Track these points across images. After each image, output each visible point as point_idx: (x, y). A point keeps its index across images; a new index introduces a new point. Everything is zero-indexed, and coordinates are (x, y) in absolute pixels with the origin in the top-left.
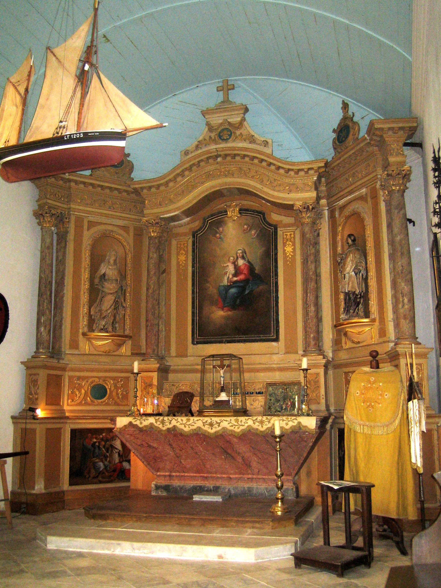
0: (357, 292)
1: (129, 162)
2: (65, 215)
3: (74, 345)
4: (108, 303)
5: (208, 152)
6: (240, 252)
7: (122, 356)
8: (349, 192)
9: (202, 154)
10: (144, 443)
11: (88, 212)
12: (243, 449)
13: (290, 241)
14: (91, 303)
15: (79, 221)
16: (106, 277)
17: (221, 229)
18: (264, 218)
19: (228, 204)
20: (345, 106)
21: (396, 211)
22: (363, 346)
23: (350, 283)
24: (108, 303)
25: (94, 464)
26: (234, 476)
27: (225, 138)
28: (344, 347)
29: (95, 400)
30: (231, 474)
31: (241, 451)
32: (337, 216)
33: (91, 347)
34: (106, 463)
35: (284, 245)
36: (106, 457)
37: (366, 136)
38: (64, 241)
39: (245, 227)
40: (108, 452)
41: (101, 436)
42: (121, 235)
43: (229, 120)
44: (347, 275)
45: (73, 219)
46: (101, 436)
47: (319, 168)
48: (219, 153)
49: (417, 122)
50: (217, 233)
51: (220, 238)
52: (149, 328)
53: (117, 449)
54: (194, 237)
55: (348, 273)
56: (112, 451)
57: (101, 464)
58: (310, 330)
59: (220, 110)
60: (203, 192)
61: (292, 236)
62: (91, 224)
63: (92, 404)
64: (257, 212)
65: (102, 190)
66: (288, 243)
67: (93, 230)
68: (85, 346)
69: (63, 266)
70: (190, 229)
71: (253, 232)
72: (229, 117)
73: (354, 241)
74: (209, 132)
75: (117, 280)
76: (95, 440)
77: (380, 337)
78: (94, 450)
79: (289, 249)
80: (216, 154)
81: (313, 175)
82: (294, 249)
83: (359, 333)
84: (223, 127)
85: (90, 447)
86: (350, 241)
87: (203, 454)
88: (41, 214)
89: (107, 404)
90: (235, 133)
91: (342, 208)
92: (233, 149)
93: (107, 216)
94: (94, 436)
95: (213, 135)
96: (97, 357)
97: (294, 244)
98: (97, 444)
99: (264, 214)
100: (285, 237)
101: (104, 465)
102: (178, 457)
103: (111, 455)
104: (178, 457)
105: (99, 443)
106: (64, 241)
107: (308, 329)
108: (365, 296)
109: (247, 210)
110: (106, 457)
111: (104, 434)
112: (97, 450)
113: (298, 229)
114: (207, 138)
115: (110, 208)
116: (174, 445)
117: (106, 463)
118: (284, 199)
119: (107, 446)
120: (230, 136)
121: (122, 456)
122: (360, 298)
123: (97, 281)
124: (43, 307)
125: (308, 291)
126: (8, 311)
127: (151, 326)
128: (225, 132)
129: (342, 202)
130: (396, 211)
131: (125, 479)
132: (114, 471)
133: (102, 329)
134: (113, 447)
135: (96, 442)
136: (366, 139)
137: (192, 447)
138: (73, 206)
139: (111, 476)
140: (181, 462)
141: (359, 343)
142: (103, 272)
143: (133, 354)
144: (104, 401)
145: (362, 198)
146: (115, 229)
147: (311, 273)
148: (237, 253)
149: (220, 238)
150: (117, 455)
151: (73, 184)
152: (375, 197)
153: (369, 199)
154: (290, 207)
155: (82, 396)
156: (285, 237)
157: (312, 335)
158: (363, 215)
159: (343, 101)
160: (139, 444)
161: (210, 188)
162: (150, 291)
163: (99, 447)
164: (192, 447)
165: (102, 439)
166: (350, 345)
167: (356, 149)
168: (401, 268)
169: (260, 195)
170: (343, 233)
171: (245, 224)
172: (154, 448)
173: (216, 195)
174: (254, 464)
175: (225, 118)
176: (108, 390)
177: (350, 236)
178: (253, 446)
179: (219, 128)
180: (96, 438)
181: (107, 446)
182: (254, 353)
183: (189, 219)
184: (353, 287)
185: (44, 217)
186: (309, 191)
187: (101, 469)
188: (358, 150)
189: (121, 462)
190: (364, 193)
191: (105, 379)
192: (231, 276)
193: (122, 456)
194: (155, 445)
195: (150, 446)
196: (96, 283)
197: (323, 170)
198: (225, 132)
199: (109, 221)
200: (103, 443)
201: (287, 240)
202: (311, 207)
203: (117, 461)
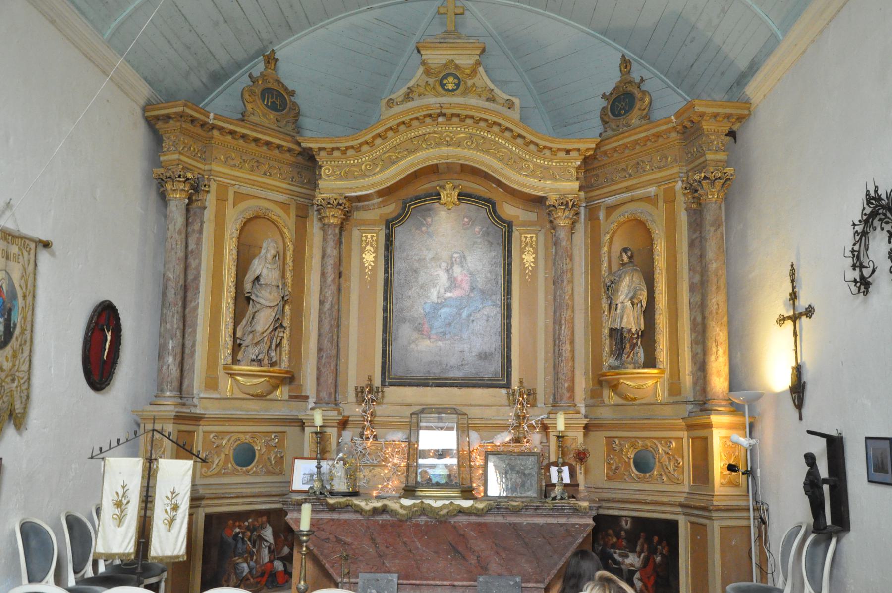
0: (634, 330)
1: (295, 104)
2: (203, 181)
3: (212, 383)
4: (264, 320)
5: (428, 107)
6: (456, 255)
7: (278, 400)
8: (627, 188)
9: (419, 108)
10: (331, 537)
11: (235, 179)
12: (480, 545)
13: (531, 247)
14: (237, 319)
15: (223, 189)
16: (262, 281)
17: (429, 220)
18: (495, 211)
19: (441, 183)
20: (626, 63)
21: (712, 229)
22: (640, 404)
23: (625, 317)
24: (264, 320)
25: (235, 566)
26: (460, 583)
27: (450, 88)
28: (606, 402)
29: (239, 468)
30: (457, 580)
31: (477, 549)
32: (601, 218)
33: (235, 387)
34: (252, 563)
35: (522, 251)
36: (251, 555)
37: (673, 117)
38: (198, 220)
39: (466, 220)
40: (254, 547)
41: (246, 523)
42: (277, 213)
43: (457, 62)
44: (620, 305)
45: (213, 187)
46: (246, 523)
47: (588, 149)
48: (443, 111)
49: (749, 108)
50: (423, 224)
51: (427, 233)
52: (323, 361)
53: (266, 541)
54: (387, 227)
55: (622, 303)
56: (260, 546)
57: (245, 565)
58: (563, 377)
59: (445, 45)
60: (412, 165)
61: (534, 239)
62: (240, 197)
63: (234, 474)
64: (484, 200)
65: (233, 138)
66: (527, 248)
67: (243, 206)
68: (227, 386)
69: (197, 261)
70: (381, 216)
71: (477, 229)
72: (457, 57)
73: (630, 258)
74: (424, 76)
75: (278, 286)
76: (238, 530)
77: (671, 394)
78: (236, 546)
79: (528, 258)
80: (439, 111)
81: (575, 159)
82: (536, 259)
83: (639, 387)
84: (447, 72)
85: (230, 540)
86: (626, 259)
87: (421, 551)
88: (170, 178)
89: (256, 473)
90: (466, 83)
91: (611, 209)
92: (466, 107)
93: (254, 183)
94: (237, 524)
95: (431, 81)
96: (243, 402)
97: (536, 252)
98: (240, 535)
99: (494, 204)
100: (523, 239)
101: (249, 566)
102: (380, 556)
103: (259, 551)
104: (380, 556)
105: (243, 533)
106: (198, 220)
107: (560, 375)
108: (648, 335)
109: (470, 196)
110: (251, 555)
111: (250, 520)
112: (240, 545)
113: (543, 231)
114: (422, 84)
115: (265, 174)
116: (378, 540)
117: (252, 563)
118: (533, 188)
119: (254, 537)
120: (458, 85)
121: (273, 552)
122: (637, 338)
123: (248, 286)
124: (172, 326)
125: (563, 322)
126: (121, 330)
127: (327, 358)
128: (451, 79)
129: (611, 200)
130: (712, 229)
131: (276, 586)
132: (263, 574)
133: (253, 361)
134: (261, 539)
135: (239, 533)
136: (671, 122)
137: (405, 543)
138: (216, 167)
139: (258, 583)
140: (384, 563)
141: (635, 399)
142: (257, 273)
143: (290, 397)
144: (252, 469)
145: (650, 200)
146: (271, 206)
147: (567, 297)
148: (452, 257)
149: (427, 233)
150: (266, 551)
151: (215, 133)
152: (670, 200)
153: (661, 203)
154: (539, 201)
155: (221, 463)
156: (523, 239)
157: (566, 385)
158: (650, 225)
159: (623, 56)
160: (323, 538)
161: (425, 160)
162: (327, 306)
163: (243, 539)
164: (405, 543)
165: (248, 528)
166: (614, 398)
167: (649, 133)
168: (715, 307)
169: (492, 176)
170: (614, 245)
171: (467, 217)
172: (345, 543)
173: (432, 170)
174: (493, 567)
175: (451, 57)
176: (257, 452)
177: (625, 250)
178: (497, 542)
179: (440, 72)
180: (239, 527)
181: (254, 537)
182: (473, 403)
183: (380, 199)
184: (628, 322)
185: (323, 217)
186: (567, 180)
187: (245, 574)
188: (653, 135)
189: (271, 561)
190: (653, 194)
191: (254, 435)
192: (442, 291)
193: (273, 552)
194: (349, 540)
195: (339, 541)
196: (247, 290)
197: (591, 152)
198: (451, 79)
199: (262, 194)
200: (249, 533)
201: (527, 245)
202: (570, 204)
203: (266, 560)
